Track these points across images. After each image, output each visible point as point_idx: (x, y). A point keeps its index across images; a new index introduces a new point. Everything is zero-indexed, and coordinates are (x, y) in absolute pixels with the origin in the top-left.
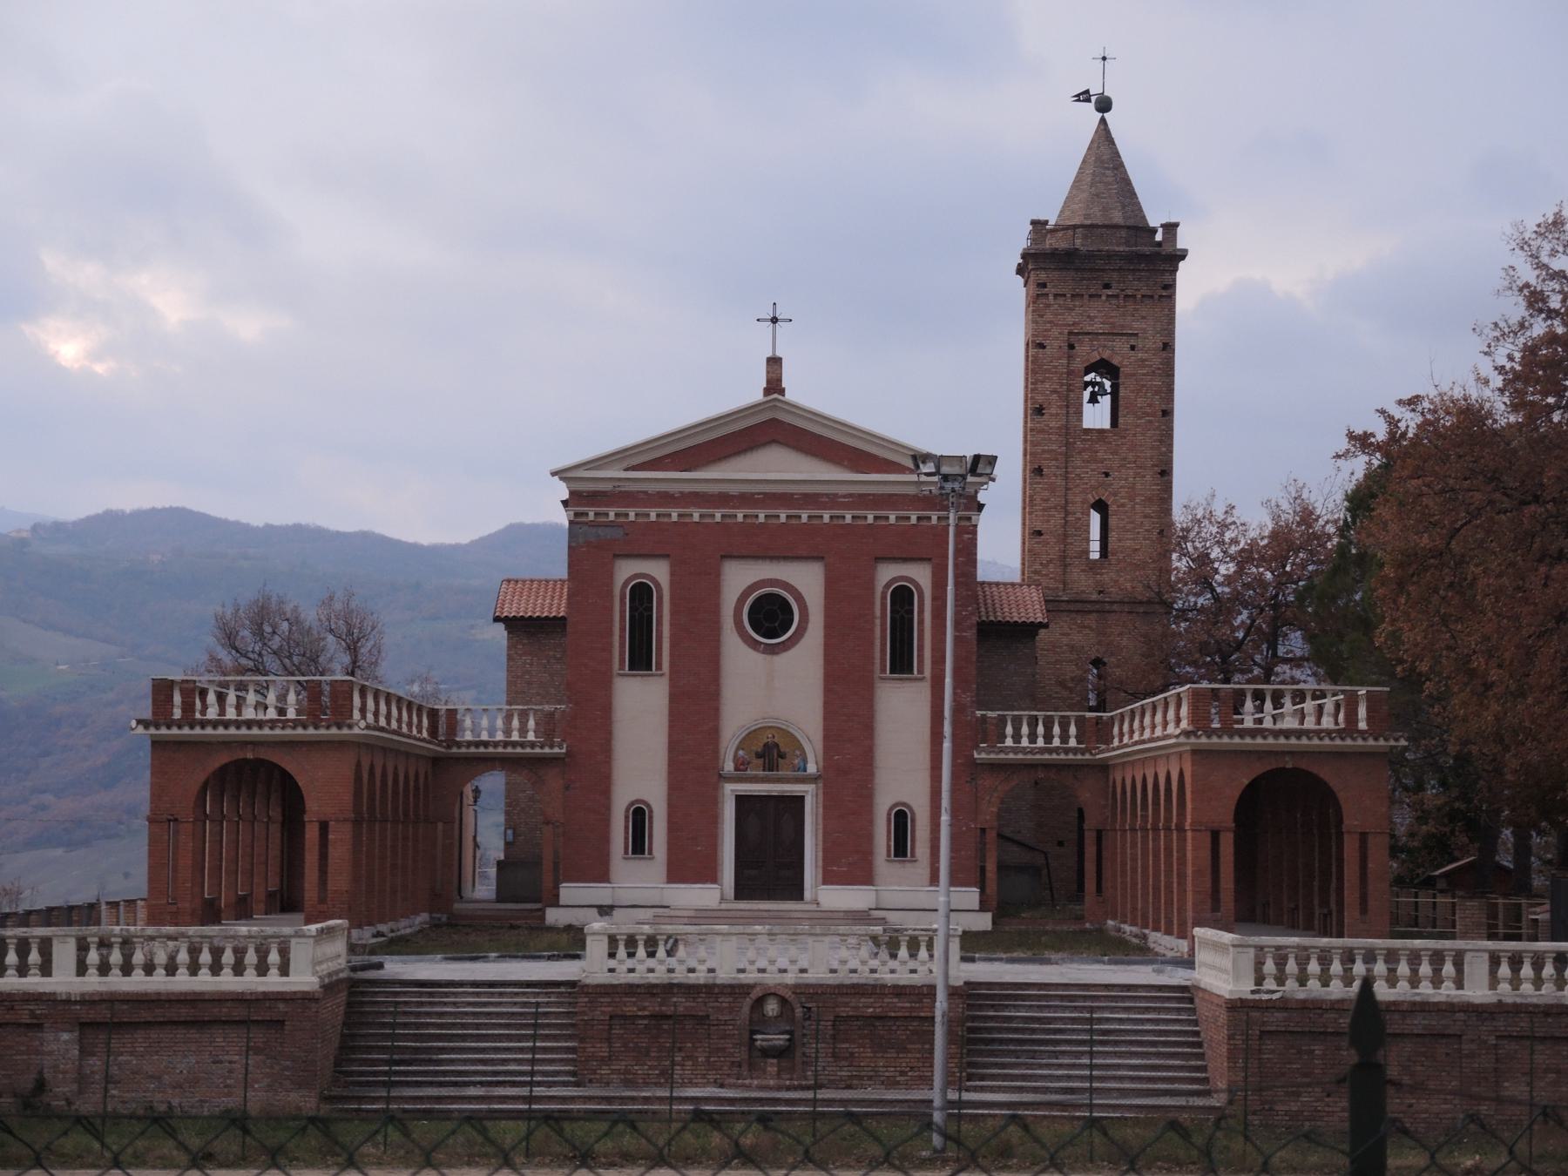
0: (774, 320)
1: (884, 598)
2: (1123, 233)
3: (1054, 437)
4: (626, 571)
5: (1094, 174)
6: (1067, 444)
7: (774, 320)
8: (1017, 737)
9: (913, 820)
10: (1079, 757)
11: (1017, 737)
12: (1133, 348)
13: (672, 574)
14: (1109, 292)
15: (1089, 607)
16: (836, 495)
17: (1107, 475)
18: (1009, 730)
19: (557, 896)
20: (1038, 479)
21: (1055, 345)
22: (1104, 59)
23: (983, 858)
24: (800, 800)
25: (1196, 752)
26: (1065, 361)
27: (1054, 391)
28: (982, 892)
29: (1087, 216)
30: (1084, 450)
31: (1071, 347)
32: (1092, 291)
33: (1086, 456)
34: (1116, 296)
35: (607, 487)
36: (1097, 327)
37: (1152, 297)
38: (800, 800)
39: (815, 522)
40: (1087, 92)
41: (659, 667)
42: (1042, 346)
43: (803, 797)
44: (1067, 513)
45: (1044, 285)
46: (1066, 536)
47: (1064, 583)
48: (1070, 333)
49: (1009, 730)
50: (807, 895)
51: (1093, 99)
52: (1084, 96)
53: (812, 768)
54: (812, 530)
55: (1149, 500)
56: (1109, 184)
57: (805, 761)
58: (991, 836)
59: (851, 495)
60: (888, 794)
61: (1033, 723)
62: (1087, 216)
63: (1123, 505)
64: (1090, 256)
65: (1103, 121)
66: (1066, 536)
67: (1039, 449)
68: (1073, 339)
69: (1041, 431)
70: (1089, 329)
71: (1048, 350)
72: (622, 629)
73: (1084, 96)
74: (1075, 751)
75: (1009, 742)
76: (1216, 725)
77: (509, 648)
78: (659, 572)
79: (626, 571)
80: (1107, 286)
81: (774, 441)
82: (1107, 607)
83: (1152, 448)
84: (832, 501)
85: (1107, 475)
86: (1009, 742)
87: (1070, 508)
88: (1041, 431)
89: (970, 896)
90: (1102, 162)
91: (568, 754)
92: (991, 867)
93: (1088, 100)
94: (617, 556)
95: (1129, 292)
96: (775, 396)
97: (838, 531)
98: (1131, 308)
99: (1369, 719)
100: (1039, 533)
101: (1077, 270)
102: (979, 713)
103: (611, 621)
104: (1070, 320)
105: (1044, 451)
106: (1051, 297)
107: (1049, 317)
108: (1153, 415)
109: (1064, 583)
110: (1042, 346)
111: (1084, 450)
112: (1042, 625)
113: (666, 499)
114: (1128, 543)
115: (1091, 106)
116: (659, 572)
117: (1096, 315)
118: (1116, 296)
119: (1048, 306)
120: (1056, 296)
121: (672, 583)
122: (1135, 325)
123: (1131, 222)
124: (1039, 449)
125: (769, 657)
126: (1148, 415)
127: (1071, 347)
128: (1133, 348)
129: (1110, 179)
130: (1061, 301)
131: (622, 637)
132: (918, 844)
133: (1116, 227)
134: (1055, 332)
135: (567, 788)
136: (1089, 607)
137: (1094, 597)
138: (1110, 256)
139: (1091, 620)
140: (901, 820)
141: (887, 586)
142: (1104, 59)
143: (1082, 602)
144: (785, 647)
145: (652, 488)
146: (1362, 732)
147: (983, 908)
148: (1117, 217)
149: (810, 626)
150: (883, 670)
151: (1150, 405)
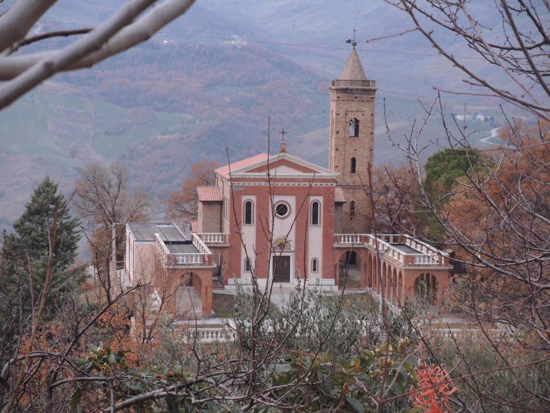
0: (283, 133)
1: (311, 205)
2: (361, 82)
3: (341, 140)
4: (245, 198)
5: (352, 65)
6: (345, 142)
7: (283, 133)
8: (344, 241)
9: (318, 262)
10: (360, 246)
11: (344, 241)
12: (363, 115)
13: (257, 199)
14: (357, 99)
15: (351, 187)
16: (299, 179)
17: (355, 150)
18: (342, 239)
19: (227, 282)
20: (337, 152)
21: (342, 114)
22: (355, 31)
23: (336, 272)
24: (289, 257)
25: (405, 270)
26: (344, 119)
27: (342, 127)
28: (336, 280)
29: (350, 77)
30: (349, 143)
31: (346, 115)
32: (352, 99)
33: (350, 145)
34: (359, 101)
35: (240, 177)
36: (353, 109)
37: (368, 101)
38: (289, 257)
39: (294, 186)
40: (350, 40)
41: (253, 223)
42: (338, 114)
43: (250, 223)
44: (345, 161)
45: (339, 97)
46: (344, 167)
47: (344, 180)
48: (346, 111)
49: (342, 239)
50: (291, 281)
51: (352, 42)
52: (349, 41)
53: (292, 249)
54: (292, 188)
55: (367, 157)
56: (356, 67)
57: (290, 247)
58: (338, 266)
59: (303, 179)
60: (311, 255)
61: (348, 237)
62: (350, 77)
63: (360, 159)
64: (352, 90)
65: (354, 48)
66: (344, 167)
67: (337, 143)
68: (347, 113)
69: (338, 138)
70: (351, 110)
71: (340, 116)
72: (244, 213)
73: (349, 41)
74: (359, 244)
75: (342, 242)
76: (410, 264)
77: (203, 208)
78: (253, 199)
79: (245, 198)
80: (356, 98)
81: (283, 165)
82: (355, 187)
83: (368, 143)
84: (298, 180)
85: (355, 150)
86: (342, 242)
87: (346, 160)
88: (338, 138)
89: (332, 281)
90: (354, 61)
91: (230, 246)
92: (338, 274)
93: (350, 42)
94: (242, 194)
95: (362, 100)
96: (284, 153)
97: (300, 188)
98: (362, 104)
99: (445, 262)
100: (337, 167)
101: (348, 93)
102: (335, 235)
103: (241, 212)
104: (346, 107)
105: (339, 144)
106: (341, 101)
107: (340, 106)
108: (368, 134)
109: (344, 180)
110: (338, 114)
111: (349, 143)
112: (344, 202)
113: (255, 180)
114: (361, 169)
115: (350, 45)
116: (253, 199)
117: (353, 106)
118: (359, 101)
119: (340, 103)
120: (342, 100)
121: (257, 202)
122: (364, 109)
123: (363, 79)
124: (337, 143)
125: (281, 220)
126: (367, 134)
127: (346, 115)
128: (363, 115)
129: (356, 66)
130: (343, 102)
131: (244, 216)
132: (319, 268)
133: (359, 81)
134: (342, 110)
135: (230, 254)
136: (351, 187)
137: (352, 184)
138: (357, 90)
139: (351, 191)
140: (315, 262)
141: (312, 202)
142: (355, 31)
143: (348, 186)
144: (286, 218)
145: (252, 177)
146: (443, 265)
147: (336, 284)
148: (359, 78)
149: (292, 212)
150: (311, 224)
151: (368, 131)
